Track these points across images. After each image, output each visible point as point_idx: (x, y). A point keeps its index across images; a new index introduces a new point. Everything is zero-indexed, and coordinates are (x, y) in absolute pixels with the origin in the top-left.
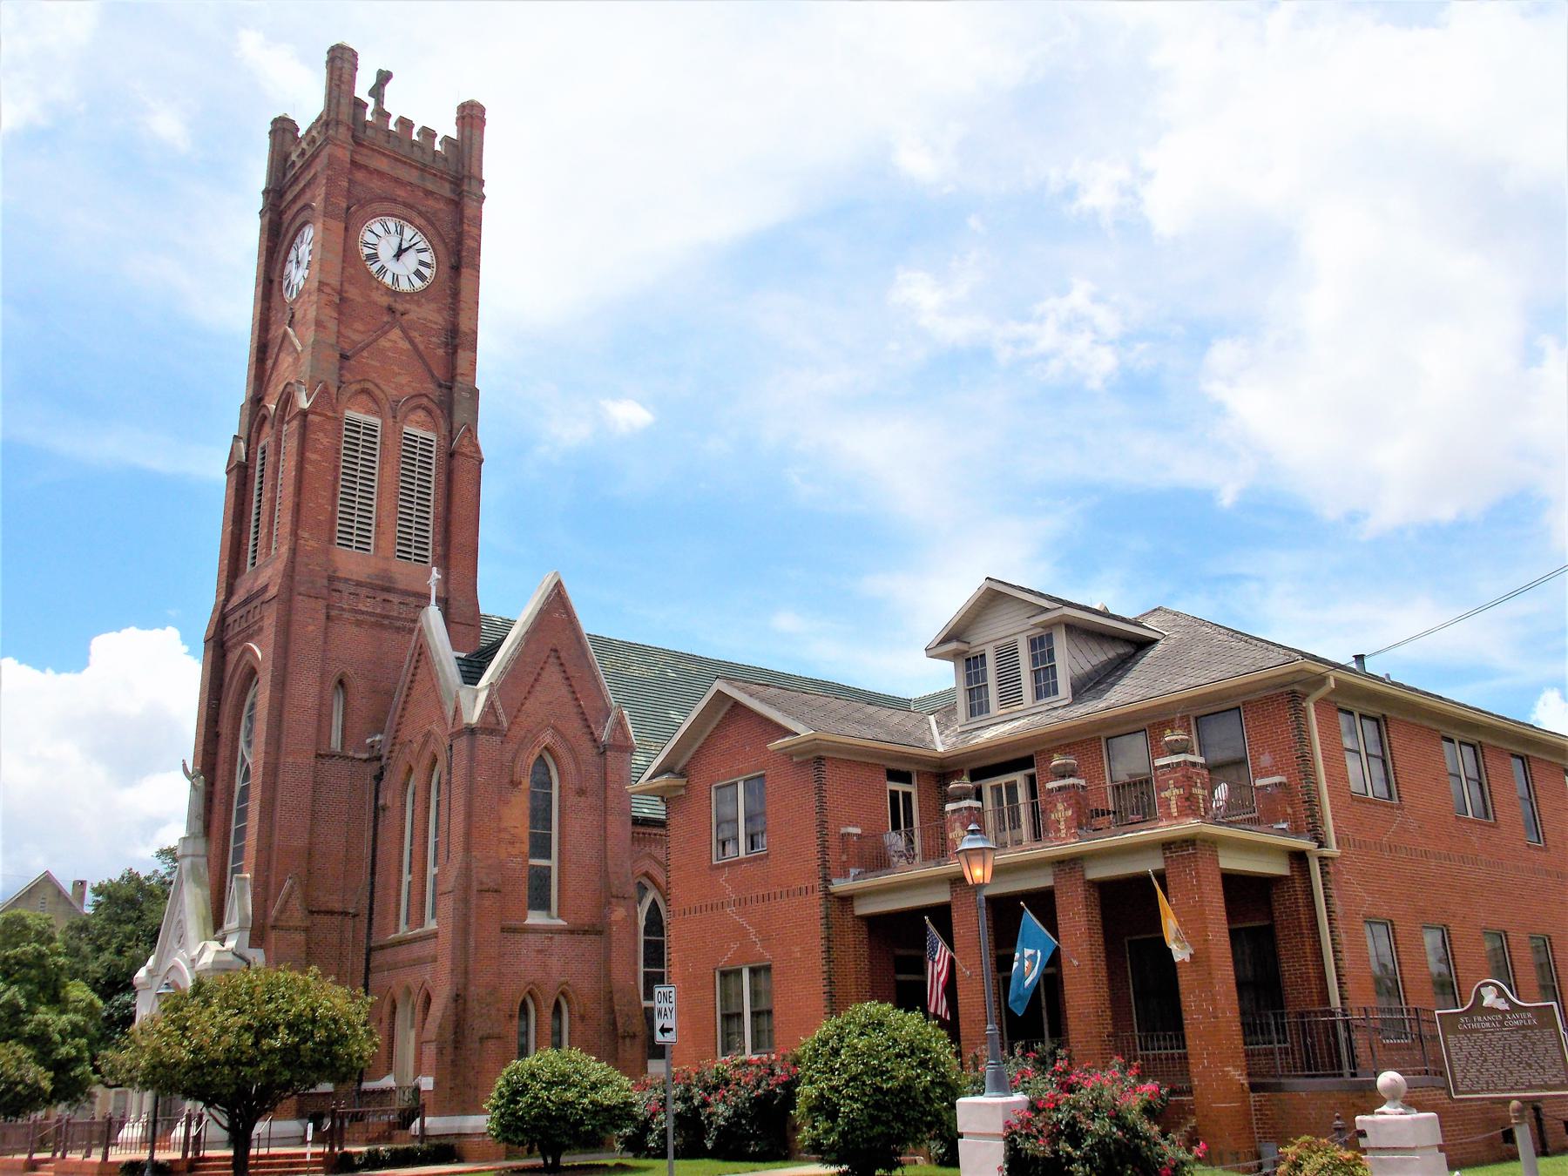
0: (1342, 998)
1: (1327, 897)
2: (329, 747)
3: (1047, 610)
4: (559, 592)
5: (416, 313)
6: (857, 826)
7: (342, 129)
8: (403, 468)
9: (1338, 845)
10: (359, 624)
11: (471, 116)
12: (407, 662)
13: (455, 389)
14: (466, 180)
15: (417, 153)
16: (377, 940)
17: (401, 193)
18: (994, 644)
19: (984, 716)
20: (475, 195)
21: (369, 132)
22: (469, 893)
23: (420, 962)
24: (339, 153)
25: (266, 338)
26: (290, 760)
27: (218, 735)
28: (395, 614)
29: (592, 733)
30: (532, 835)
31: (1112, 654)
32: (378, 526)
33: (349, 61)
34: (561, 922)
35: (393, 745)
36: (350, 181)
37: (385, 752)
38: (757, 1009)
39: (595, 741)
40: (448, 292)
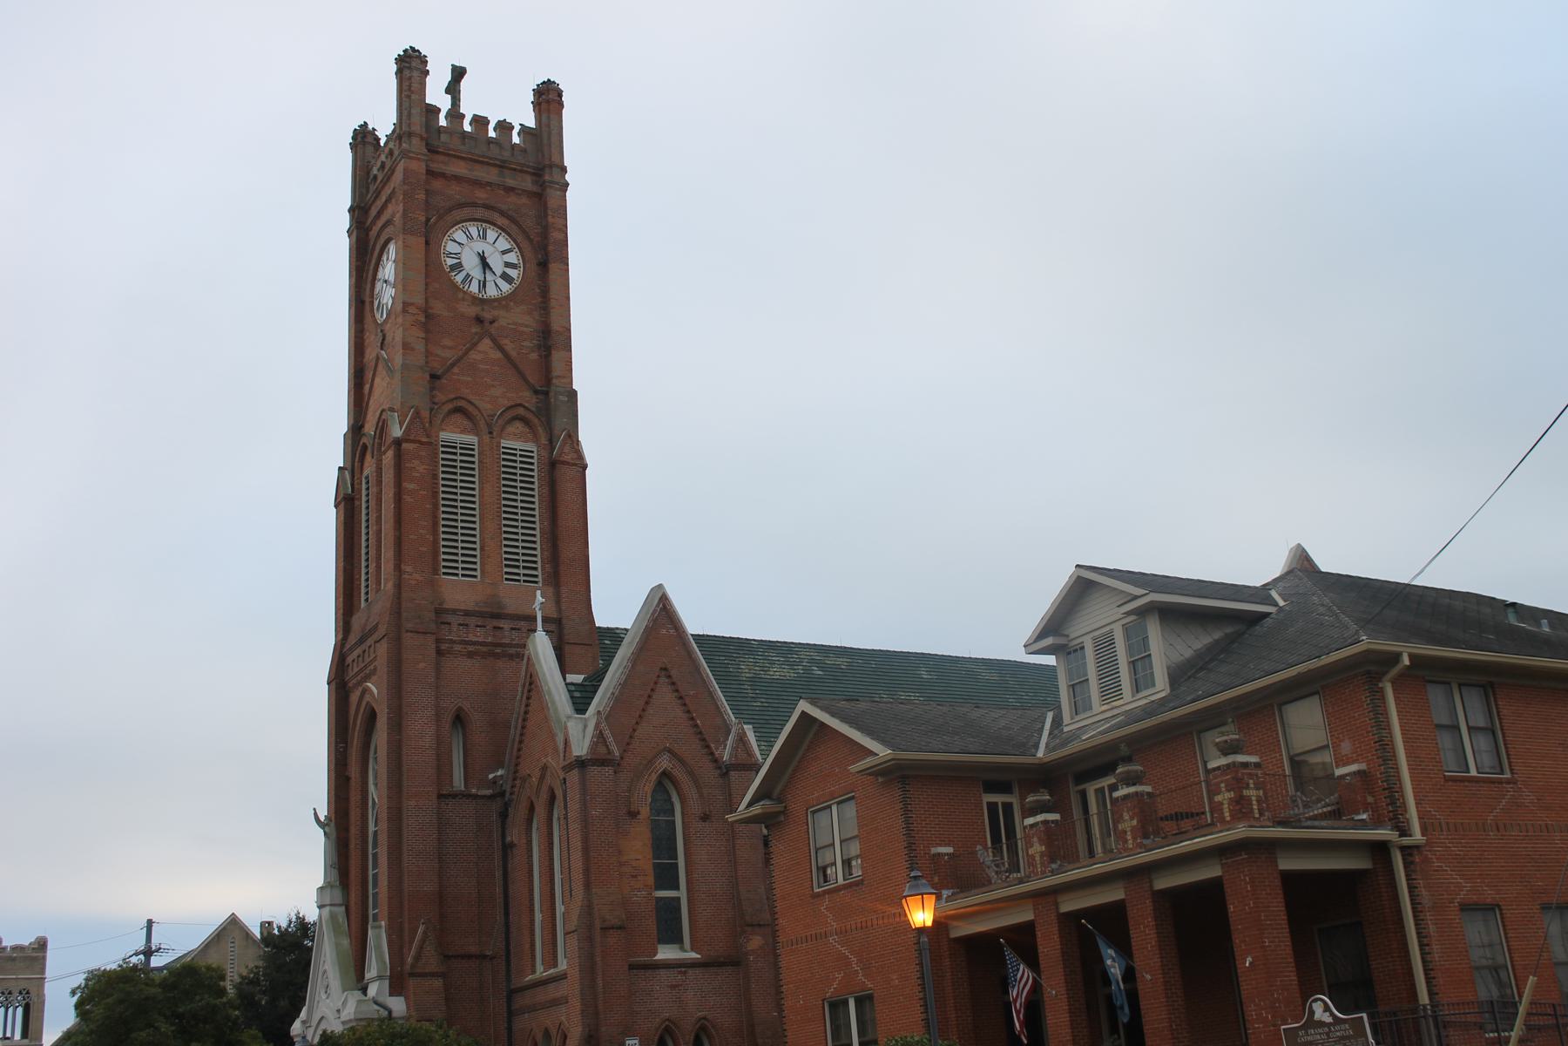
0: (1431, 994)
1: (1411, 888)
2: (452, 787)
3: (1136, 598)
4: (664, 605)
5: (506, 319)
6: (949, 845)
7: (415, 141)
8: (504, 485)
9: (1424, 831)
10: (470, 655)
11: (548, 98)
12: (520, 693)
13: (552, 394)
14: (547, 170)
15: (494, 151)
16: (515, 984)
17: (481, 195)
18: (1092, 635)
19: (1088, 714)
20: (557, 184)
21: (444, 137)
22: (591, 931)
23: (556, 1003)
24: (414, 165)
25: (362, 362)
26: (413, 803)
27: (348, 779)
28: (507, 641)
29: (712, 754)
30: (656, 866)
31: (1217, 635)
32: (482, 549)
33: (417, 69)
34: (694, 955)
35: (514, 779)
36: (427, 192)
37: (508, 788)
38: (867, 1039)
39: (716, 761)
40: (538, 291)
